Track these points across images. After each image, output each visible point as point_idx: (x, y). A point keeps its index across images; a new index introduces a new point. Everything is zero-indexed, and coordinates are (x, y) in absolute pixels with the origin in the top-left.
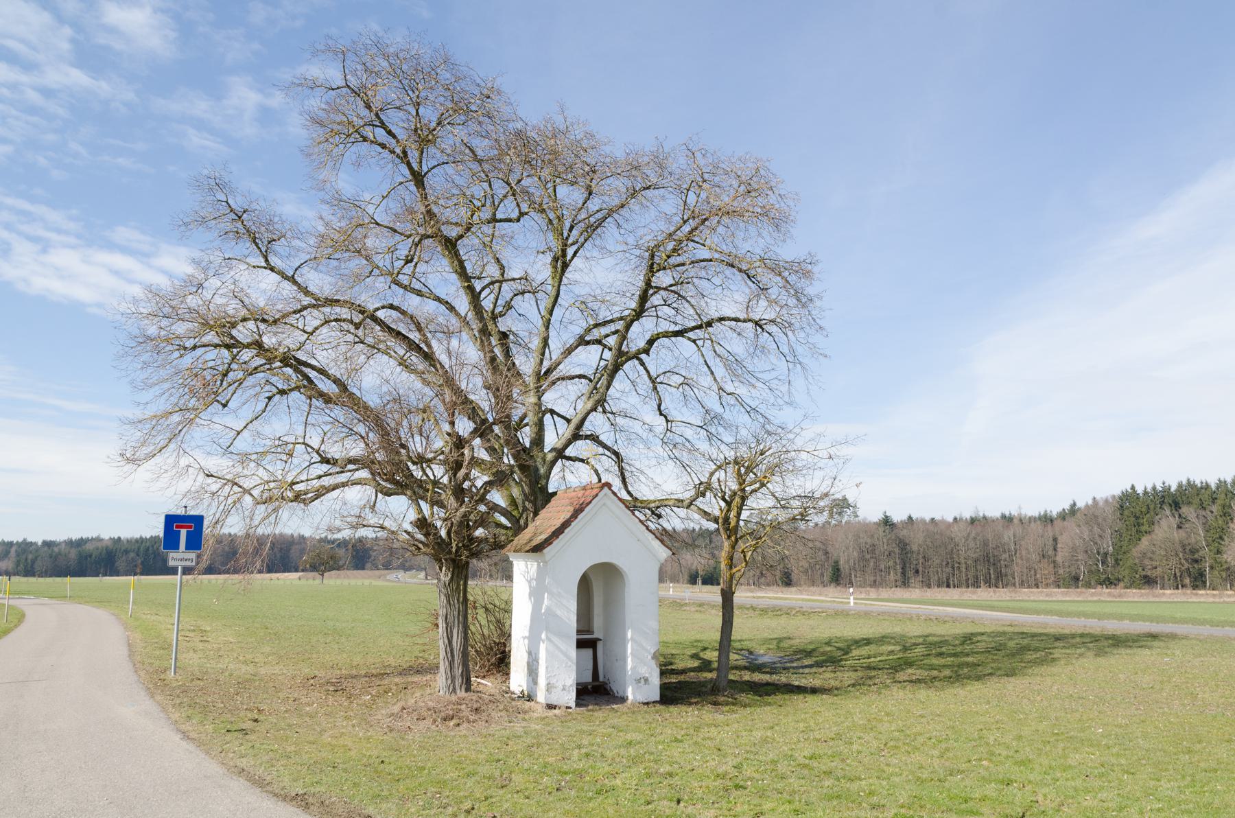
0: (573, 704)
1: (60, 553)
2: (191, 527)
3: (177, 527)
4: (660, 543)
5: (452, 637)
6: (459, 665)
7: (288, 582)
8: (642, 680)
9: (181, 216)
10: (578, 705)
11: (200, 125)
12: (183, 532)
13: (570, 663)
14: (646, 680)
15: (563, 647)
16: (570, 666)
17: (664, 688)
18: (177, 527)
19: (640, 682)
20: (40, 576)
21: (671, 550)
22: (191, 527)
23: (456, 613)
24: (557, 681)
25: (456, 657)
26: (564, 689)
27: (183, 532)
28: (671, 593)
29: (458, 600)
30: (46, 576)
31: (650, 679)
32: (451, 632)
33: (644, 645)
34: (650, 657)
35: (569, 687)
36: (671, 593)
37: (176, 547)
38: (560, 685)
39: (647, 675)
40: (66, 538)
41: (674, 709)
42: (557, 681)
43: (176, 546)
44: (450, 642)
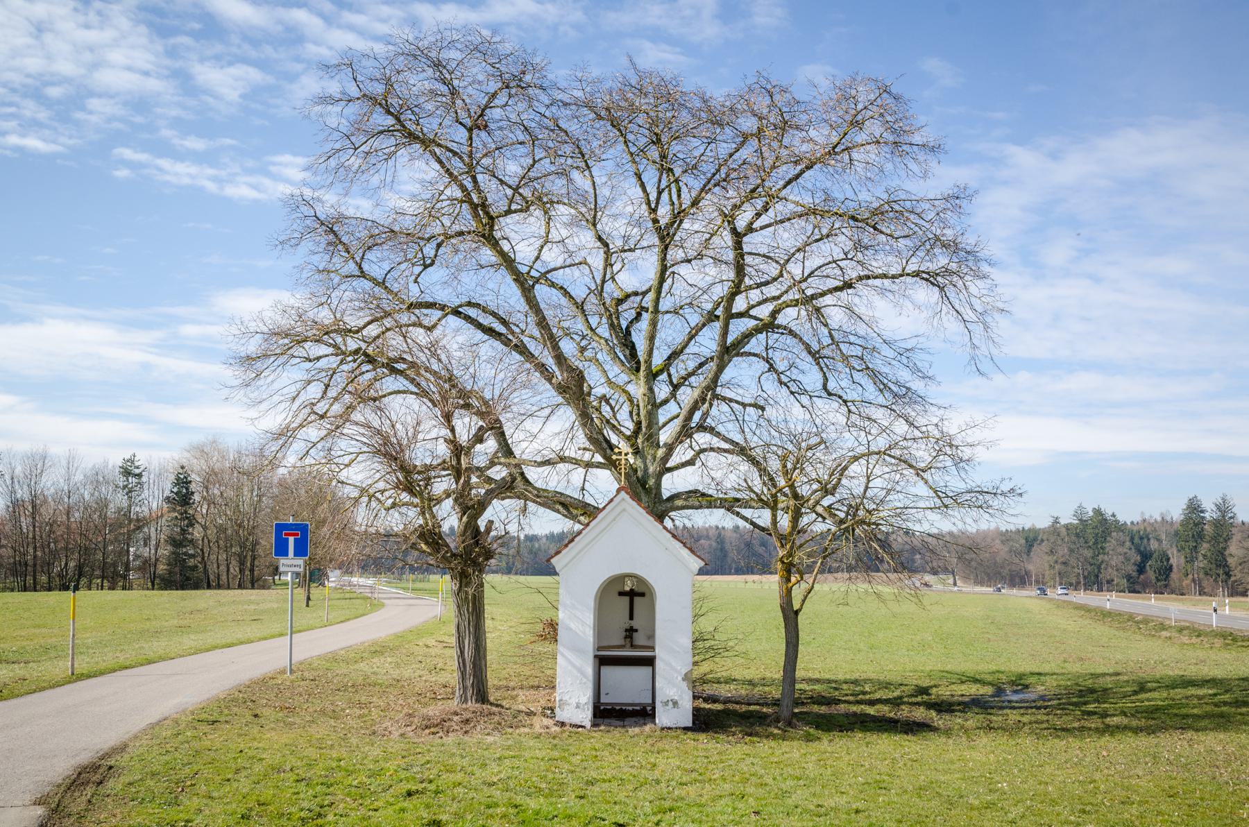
0: (588, 724)
1: (539, 549)
2: (297, 535)
3: (286, 534)
4: (689, 552)
5: (464, 647)
6: (470, 675)
7: (766, 587)
8: (671, 703)
9: (275, 236)
10: (594, 725)
11: (657, 36)
12: (291, 540)
13: (585, 680)
14: (675, 703)
15: (578, 662)
16: (585, 683)
17: (697, 713)
18: (286, 534)
19: (667, 705)
20: (739, 571)
21: (702, 559)
22: (297, 535)
23: (466, 623)
24: (570, 698)
25: (468, 669)
26: (578, 707)
27: (291, 540)
28: (1227, 612)
29: (468, 610)
30: (528, 575)
31: (680, 703)
32: (463, 642)
33: (673, 664)
34: (680, 678)
35: (584, 705)
36: (1227, 612)
37: (286, 554)
38: (573, 701)
39: (676, 698)
40: (548, 532)
41: (702, 737)
42: (570, 698)
43: (286, 554)
44: (462, 652)
